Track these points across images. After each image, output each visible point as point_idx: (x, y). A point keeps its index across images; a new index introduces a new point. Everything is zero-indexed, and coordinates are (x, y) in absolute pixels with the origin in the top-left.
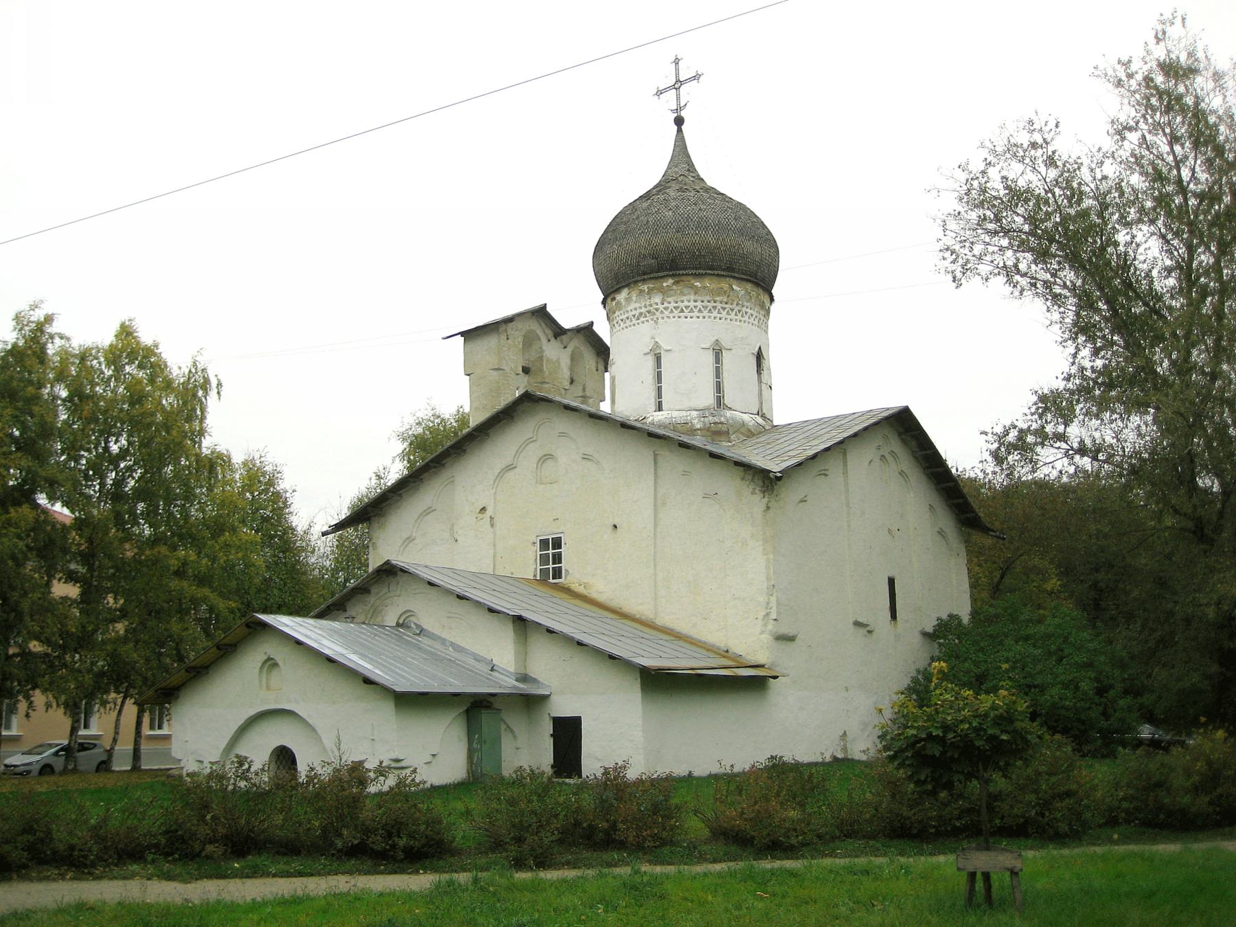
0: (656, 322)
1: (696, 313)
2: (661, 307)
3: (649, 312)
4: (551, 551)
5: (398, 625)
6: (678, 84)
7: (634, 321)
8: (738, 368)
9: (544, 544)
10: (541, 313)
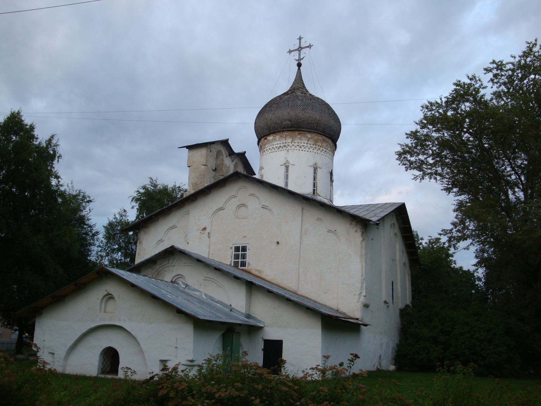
0: (288, 151)
1: (307, 149)
2: (291, 144)
3: (285, 146)
4: (240, 253)
5: (172, 282)
6: (300, 49)
7: (276, 150)
8: (322, 175)
9: (237, 249)
10: (225, 143)
